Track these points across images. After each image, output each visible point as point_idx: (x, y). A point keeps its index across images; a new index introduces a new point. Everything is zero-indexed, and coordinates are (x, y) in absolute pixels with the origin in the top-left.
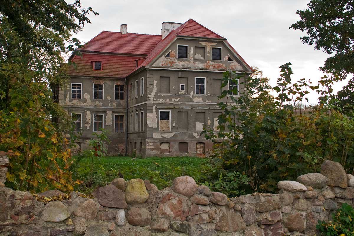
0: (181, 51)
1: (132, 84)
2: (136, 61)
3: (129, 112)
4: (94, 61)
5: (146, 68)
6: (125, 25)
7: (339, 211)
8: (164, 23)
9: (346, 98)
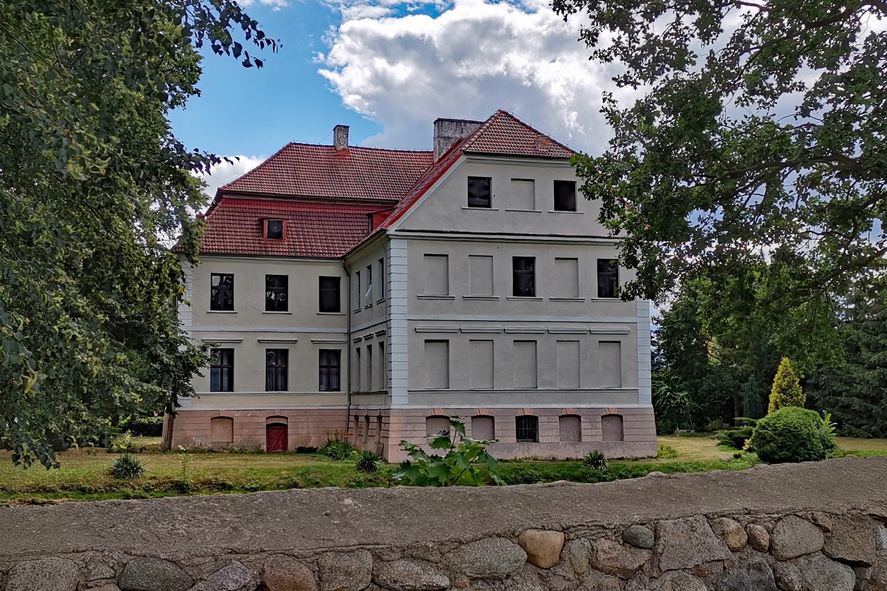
0: (474, 191)
1: (358, 273)
2: (370, 216)
3: (352, 342)
4: (267, 218)
5: (388, 233)
6: (345, 127)
7: (878, 178)
8: (439, 120)
9: (879, 137)
